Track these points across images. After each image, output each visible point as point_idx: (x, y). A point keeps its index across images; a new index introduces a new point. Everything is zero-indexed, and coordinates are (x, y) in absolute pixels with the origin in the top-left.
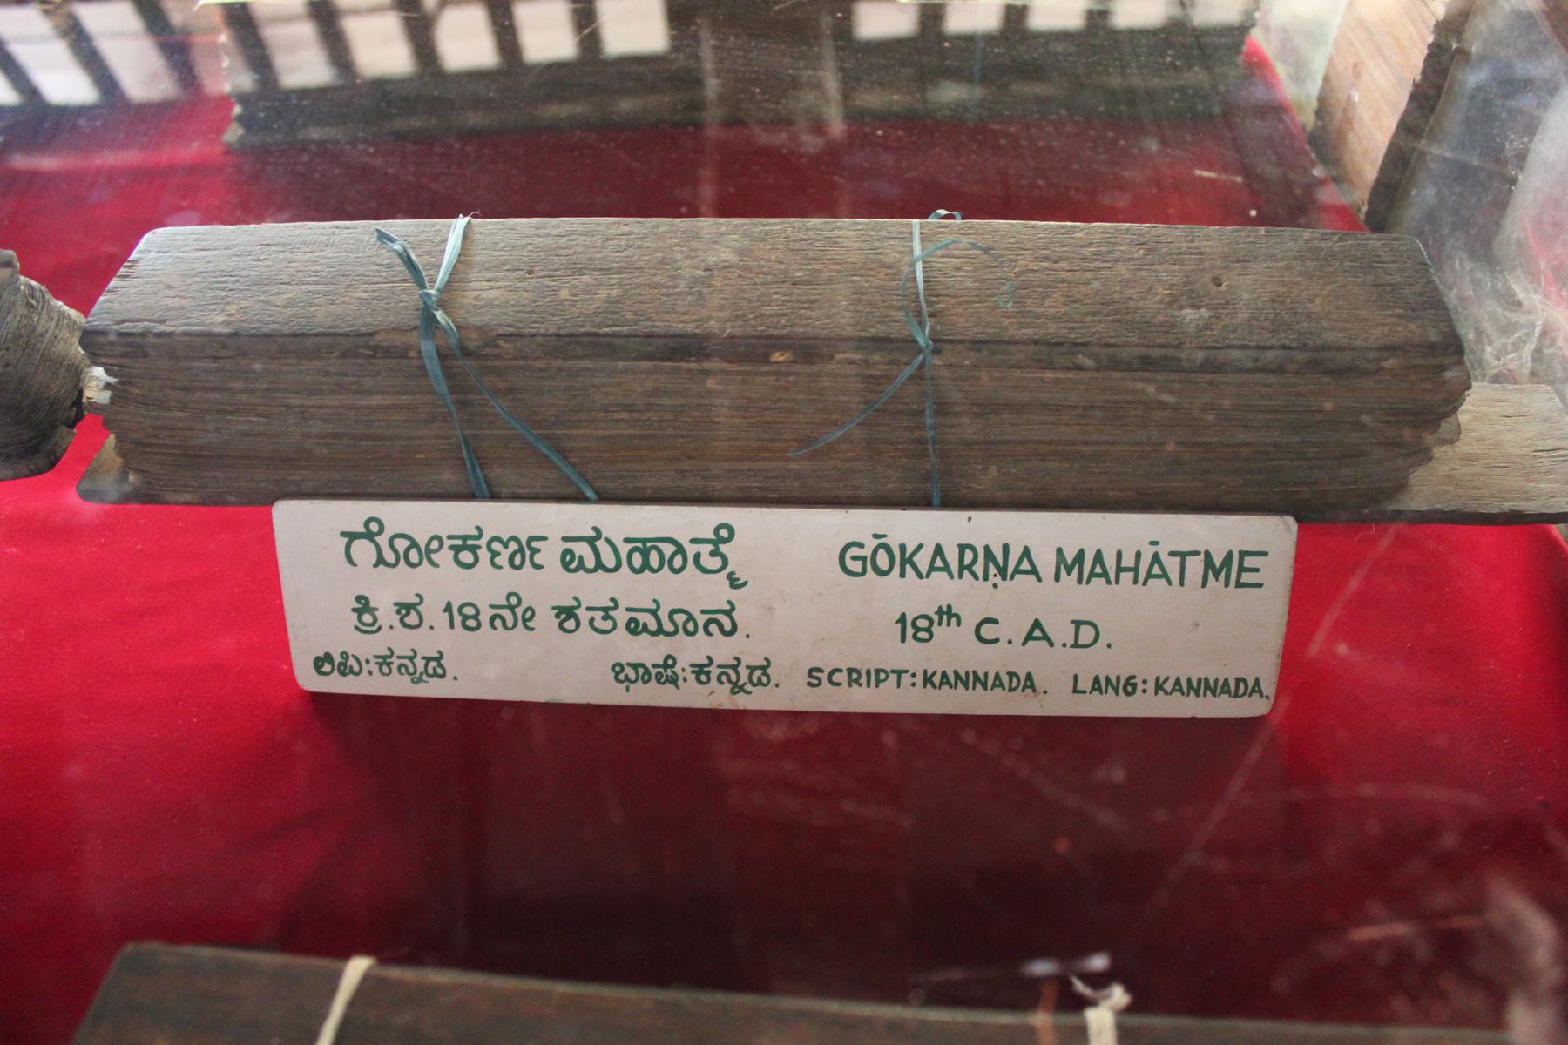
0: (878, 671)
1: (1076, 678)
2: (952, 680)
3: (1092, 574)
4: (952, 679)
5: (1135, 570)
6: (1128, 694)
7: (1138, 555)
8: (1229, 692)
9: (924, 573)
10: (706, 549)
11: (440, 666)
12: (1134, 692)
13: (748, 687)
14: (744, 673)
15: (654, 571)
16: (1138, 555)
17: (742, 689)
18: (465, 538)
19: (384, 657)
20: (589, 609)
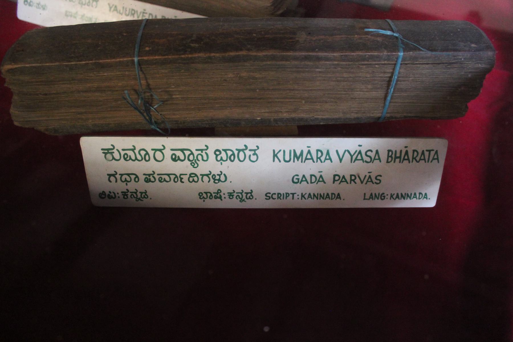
0: (286, 193)
1: (365, 194)
2: (312, 197)
5: (400, 157)
6: (382, 199)
8: (416, 197)
9: (323, 161)
11: (146, 195)
12: (384, 199)
13: (246, 200)
14: (244, 195)
16: (401, 151)
17: (244, 200)
19: (231, 193)
20: (158, 175)
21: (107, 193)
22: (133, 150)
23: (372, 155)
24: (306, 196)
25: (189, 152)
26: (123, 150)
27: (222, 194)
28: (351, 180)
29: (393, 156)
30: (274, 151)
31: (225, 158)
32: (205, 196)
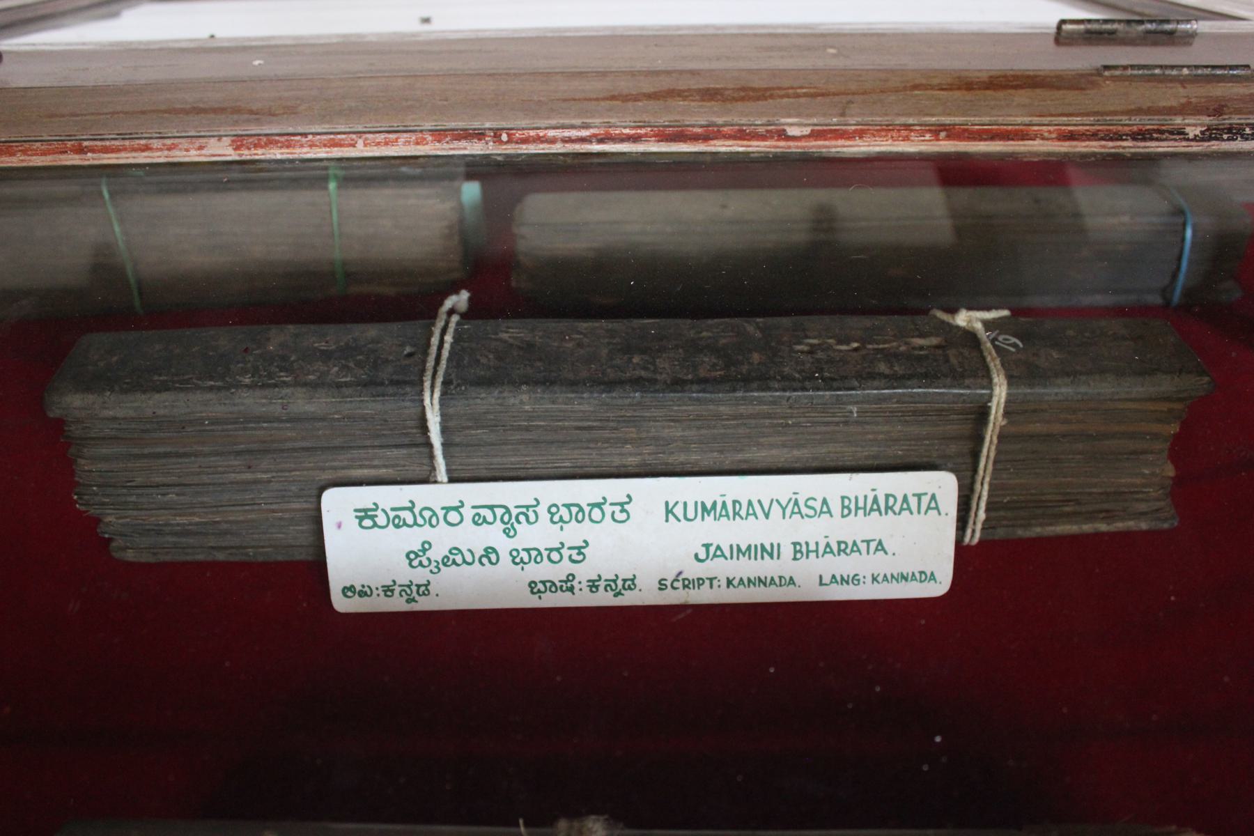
0: (699, 579)
1: (821, 577)
3: (721, 516)
4: (839, 579)
7: (866, 497)
10: (618, 508)
13: (417, 598)
14: (620, 583)
15: (360, 525)
16: (866, 497)
18: (365, 510)
19: (593, 581)
21: (358, 588)
22: (411, 509)
23: (817, 505)
24: (880, 579)
25: (430, 513)
26: (393, 509)
27: (575, 583)
28: (839, 550)
29: (852, 506)
30: (667, 503)
31: (566, 518)
32: (542, 589)
